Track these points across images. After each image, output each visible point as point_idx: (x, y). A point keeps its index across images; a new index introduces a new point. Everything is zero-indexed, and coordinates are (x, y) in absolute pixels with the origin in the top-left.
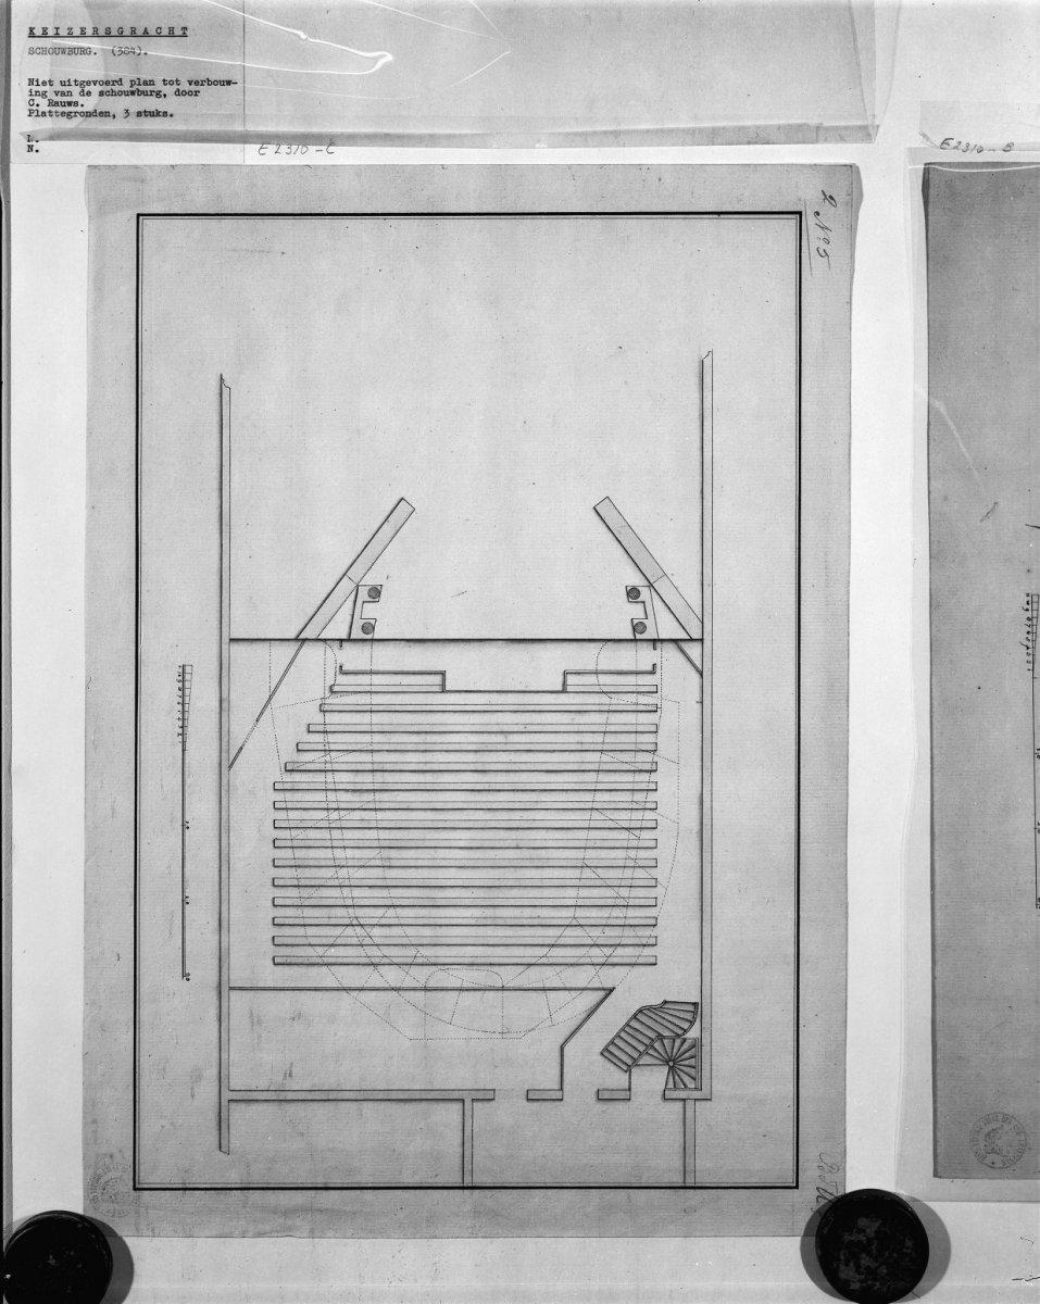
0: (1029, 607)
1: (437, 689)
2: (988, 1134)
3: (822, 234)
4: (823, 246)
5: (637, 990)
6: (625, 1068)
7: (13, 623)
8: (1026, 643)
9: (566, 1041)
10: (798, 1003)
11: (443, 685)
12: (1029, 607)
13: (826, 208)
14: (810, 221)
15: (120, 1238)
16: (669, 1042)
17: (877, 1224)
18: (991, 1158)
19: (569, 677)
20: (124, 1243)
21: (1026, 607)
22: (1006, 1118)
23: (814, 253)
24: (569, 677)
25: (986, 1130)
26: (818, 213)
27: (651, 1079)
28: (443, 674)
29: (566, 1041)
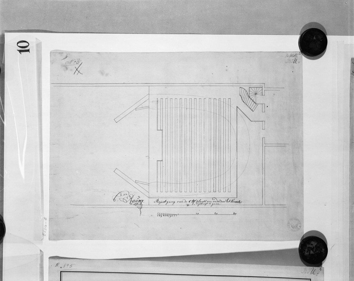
0: (161, 215)
1: (161, 162)
2: (293, 227)
3: (66, 266)
4: (69, 266)
5: (237, 101)
6: (256, 106)
7: (125, 34)
8: (170, 216)
9: (250, 120)
10: (261, 277)
11: (161, 161)
12: (161, 215)
13: (60, 265)
14: (62, 270)
15: (304, 235)
16: (250, 95)
17: (316, 244)
18: (298, 227)
19: (158, 129)
20: (305, 234)
21: (161, 216)
22: (289, 223)
23: (71, 268)
24: (158, 129)
25: (291, 228)
26: (61, 267)
27: (259, 99)
28: (158, 161)
29: (250, 120)
